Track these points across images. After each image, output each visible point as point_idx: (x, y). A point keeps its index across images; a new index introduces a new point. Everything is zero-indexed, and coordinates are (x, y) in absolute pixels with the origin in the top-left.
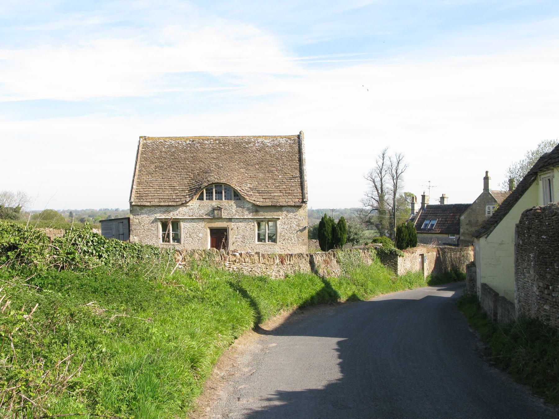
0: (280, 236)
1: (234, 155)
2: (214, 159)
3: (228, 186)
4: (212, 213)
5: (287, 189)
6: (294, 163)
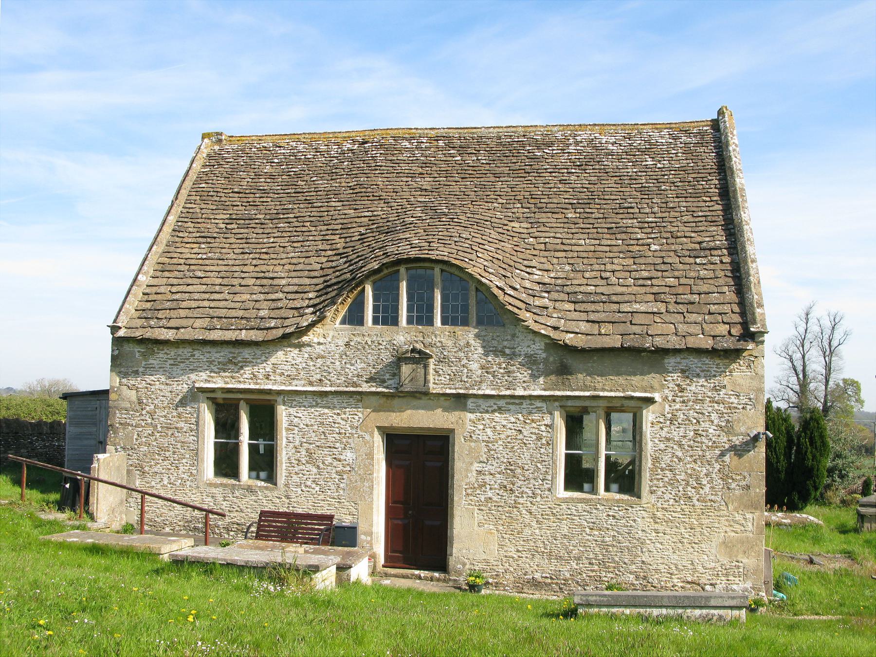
0: (653, 470)
1: (493, 179)
2: (423, 193)
3: (457, 272)
4: (394, 375)
5: (680, 290)
6: (703, 204)
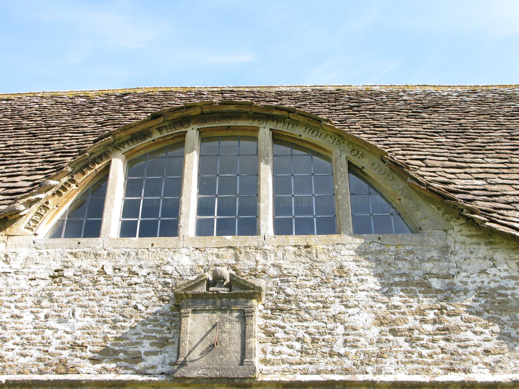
4: (163, 343)
